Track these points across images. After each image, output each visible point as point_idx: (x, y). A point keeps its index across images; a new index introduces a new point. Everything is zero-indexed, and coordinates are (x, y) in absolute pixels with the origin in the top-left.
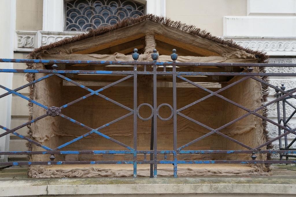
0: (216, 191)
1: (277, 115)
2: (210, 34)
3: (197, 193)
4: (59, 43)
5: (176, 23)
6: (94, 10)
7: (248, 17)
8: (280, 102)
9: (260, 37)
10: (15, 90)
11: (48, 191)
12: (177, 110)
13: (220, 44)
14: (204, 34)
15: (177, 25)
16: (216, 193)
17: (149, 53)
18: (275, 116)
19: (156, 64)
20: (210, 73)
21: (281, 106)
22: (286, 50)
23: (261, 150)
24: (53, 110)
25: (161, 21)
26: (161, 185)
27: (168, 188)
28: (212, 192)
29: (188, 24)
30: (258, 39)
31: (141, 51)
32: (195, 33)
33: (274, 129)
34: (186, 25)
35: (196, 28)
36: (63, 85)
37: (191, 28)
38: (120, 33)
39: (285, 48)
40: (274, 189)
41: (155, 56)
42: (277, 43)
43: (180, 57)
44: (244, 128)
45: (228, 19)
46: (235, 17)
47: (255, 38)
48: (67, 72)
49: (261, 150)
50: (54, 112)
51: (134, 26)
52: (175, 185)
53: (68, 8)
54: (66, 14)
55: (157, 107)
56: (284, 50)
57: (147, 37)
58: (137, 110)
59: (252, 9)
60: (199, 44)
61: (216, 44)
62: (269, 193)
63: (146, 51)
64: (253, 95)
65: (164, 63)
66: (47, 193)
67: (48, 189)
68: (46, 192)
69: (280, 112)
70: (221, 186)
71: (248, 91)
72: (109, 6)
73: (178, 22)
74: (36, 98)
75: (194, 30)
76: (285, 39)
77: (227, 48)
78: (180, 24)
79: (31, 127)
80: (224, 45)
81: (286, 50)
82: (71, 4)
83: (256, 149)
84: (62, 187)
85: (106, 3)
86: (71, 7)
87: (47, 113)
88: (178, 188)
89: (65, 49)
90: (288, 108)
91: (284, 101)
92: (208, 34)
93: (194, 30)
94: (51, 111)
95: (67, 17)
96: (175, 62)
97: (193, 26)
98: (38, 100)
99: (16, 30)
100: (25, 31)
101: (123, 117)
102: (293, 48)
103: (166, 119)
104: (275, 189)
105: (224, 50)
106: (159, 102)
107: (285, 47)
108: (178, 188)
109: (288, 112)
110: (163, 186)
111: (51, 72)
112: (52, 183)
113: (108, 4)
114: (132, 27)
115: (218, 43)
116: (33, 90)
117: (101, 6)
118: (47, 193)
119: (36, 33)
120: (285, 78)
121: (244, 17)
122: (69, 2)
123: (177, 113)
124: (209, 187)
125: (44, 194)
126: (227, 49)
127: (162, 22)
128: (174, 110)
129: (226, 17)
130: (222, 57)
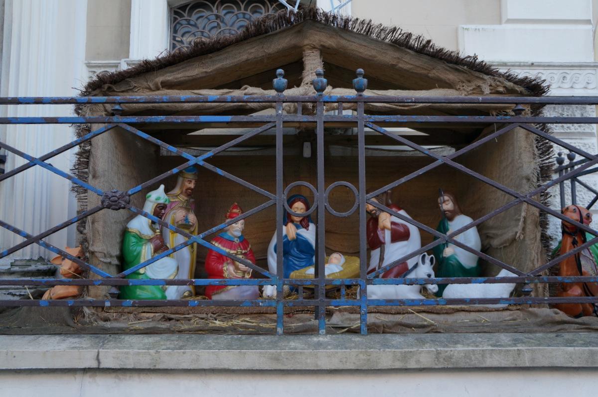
0: (448, 364)
1: (560, 206)
2: (431, 44)
3: (409, 367)
4: (133, 70)
5: (363, 23)
6: (223, 22)
7: (505, 26)
8: (565, 182)
9: (527, 63)
10: (42, 157)
11: (101, 361)
12: (367, 193)
13: (451, 65)
14: (421, 44)
15: (366, 27)
16: (449, 367)
17: (309, 83)
18: (556, 208)
19: (321, 100)
20: (435, 118)
21: (568, 190)
22: (576, 86)
23: (541, 276)
24: (114, 196)
25: (333, 22)
26: (332, 352)
27: (346, 358)
28: (440, 366)
29: (388, 24)
30: (524, 66)
31: (295, 80)
32: (402, 44)
33: (554, 233)
34: (382, 28)
35: (403, 32)
36: (161, 155)
37: (393, 34)
38: (253, 48)
39: (572, 83)
40: (569, 357)
41: (320, 84)
42: (558, 74)
43: (373, 92)
44: (501, 235)
45: (467, 29)
46: (480, 27)
47: (518, 64)
48: (142, 120)
49: (541, 276)
50: (116, 201)
51: (280, 32)
52: (361, 352)
53: (175, 19)
54: (172, 30)
55: (325, 190)
56: (572, 87)
57: (307, 52)
58: (283, 195)
59: (512, 10)
60: (412, 66)
61: (444, 66)
62: (559, 365)
63: (304, 79)
64: (520, 167)
65: (338, 99)
66: (99, 365)
67: (100, 357)
68: (97, 362)
69: (566, 201)
70: (459, 352)
71: (510, 160)
72: (248, 12)
73: (367, 21)
74: (94, 177)
75: (398, 38)
76: (572, 66)
77: (465, 73)
78: (370, 26)
79: (85, 231)
80: (460, 67)
81: (576, 86)
82: (181, 12)
83: (532, 274)
84: (127, 353)
85: (242, 7)
86: (181, 17)
87: (103, 202)
88: (369, 357)
89: (147, 82)
90: (580, 193)
91: (574, 179)
92: (429, 42)
93: (400, 36)
94: (110, 198)
95: (175, 35)
96: (361, 95)
97: (397, 29)
98: (97, 181)
99: (86, 60)
100: (100, 62)
101: (254, 211)
102: (588, 83)
103: (344, 214)
104: (571, 357)
105: (461, 78)
106: (329, 179)
107: (574, 80)
108: (369, 357)
109: (580, 200)
110: (337, 353)
111: (111, 121)
112: (112, 344)
113: (246, 9)
114: (276, 34)
115: (448, 63)
116: (88, 162)
117: (233, 13)
118: (99, 365)
119: (119, 65)
120: (574, 139)
121: (497, 27)
122: (179, 8)
123: (367, 200)
124: (434, 356)
125: (92, 367)
126: (465, 75)
127: (335, 24)
128: (360, 196)
129: (463, 26)
130: (457, 90)
